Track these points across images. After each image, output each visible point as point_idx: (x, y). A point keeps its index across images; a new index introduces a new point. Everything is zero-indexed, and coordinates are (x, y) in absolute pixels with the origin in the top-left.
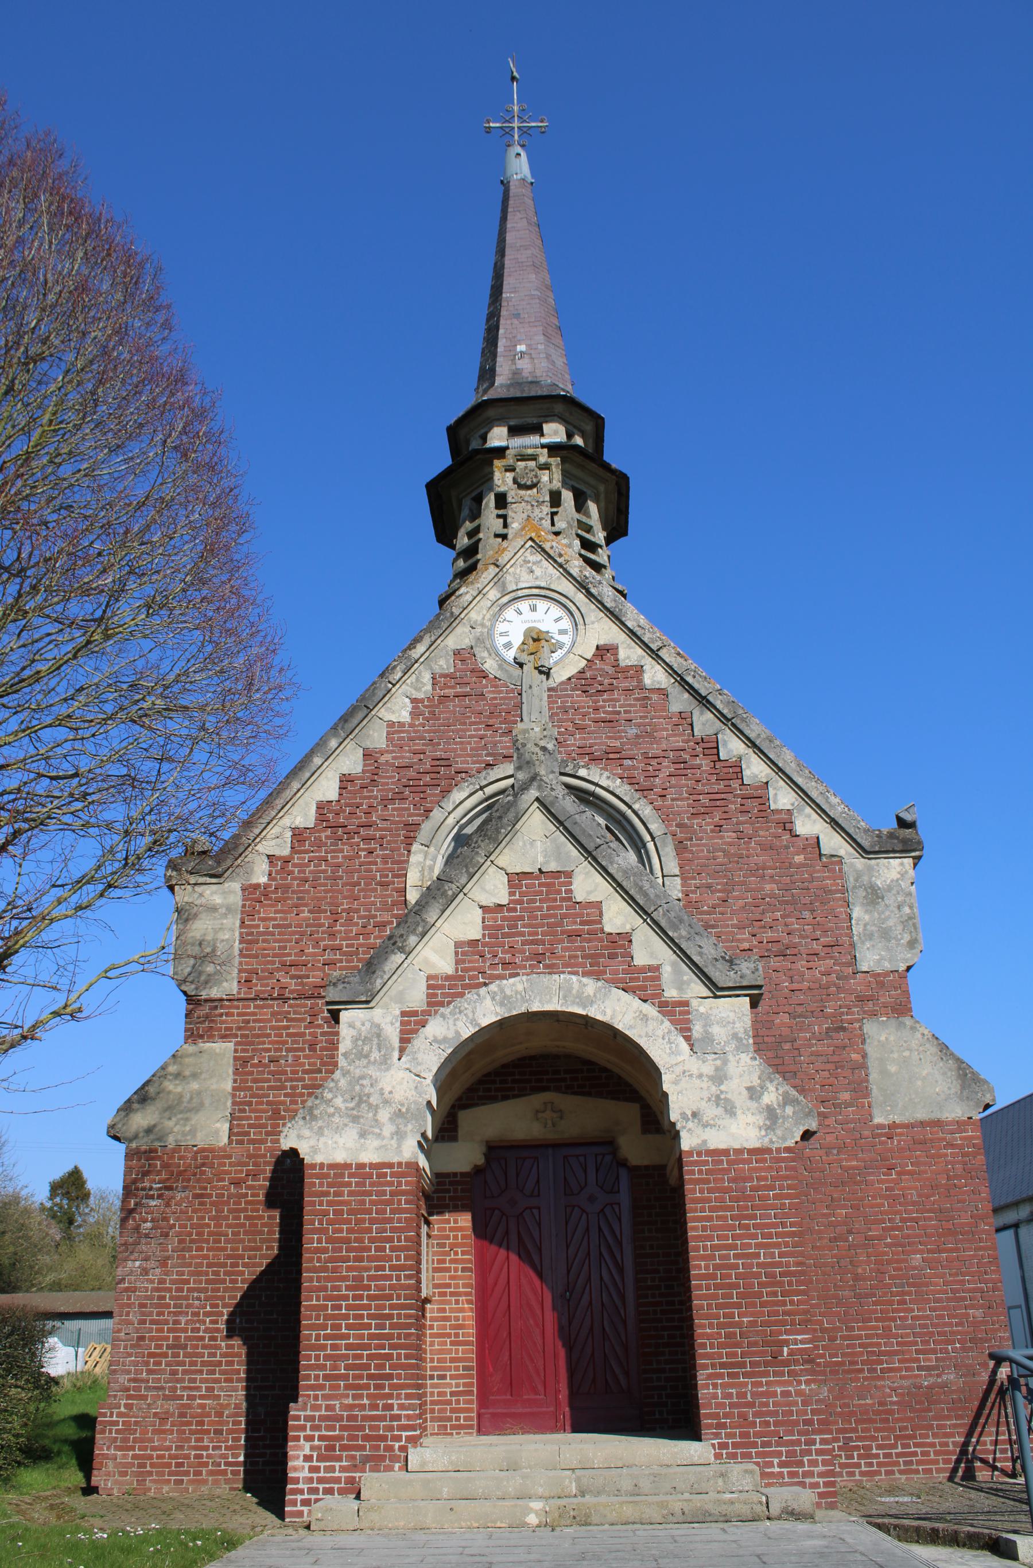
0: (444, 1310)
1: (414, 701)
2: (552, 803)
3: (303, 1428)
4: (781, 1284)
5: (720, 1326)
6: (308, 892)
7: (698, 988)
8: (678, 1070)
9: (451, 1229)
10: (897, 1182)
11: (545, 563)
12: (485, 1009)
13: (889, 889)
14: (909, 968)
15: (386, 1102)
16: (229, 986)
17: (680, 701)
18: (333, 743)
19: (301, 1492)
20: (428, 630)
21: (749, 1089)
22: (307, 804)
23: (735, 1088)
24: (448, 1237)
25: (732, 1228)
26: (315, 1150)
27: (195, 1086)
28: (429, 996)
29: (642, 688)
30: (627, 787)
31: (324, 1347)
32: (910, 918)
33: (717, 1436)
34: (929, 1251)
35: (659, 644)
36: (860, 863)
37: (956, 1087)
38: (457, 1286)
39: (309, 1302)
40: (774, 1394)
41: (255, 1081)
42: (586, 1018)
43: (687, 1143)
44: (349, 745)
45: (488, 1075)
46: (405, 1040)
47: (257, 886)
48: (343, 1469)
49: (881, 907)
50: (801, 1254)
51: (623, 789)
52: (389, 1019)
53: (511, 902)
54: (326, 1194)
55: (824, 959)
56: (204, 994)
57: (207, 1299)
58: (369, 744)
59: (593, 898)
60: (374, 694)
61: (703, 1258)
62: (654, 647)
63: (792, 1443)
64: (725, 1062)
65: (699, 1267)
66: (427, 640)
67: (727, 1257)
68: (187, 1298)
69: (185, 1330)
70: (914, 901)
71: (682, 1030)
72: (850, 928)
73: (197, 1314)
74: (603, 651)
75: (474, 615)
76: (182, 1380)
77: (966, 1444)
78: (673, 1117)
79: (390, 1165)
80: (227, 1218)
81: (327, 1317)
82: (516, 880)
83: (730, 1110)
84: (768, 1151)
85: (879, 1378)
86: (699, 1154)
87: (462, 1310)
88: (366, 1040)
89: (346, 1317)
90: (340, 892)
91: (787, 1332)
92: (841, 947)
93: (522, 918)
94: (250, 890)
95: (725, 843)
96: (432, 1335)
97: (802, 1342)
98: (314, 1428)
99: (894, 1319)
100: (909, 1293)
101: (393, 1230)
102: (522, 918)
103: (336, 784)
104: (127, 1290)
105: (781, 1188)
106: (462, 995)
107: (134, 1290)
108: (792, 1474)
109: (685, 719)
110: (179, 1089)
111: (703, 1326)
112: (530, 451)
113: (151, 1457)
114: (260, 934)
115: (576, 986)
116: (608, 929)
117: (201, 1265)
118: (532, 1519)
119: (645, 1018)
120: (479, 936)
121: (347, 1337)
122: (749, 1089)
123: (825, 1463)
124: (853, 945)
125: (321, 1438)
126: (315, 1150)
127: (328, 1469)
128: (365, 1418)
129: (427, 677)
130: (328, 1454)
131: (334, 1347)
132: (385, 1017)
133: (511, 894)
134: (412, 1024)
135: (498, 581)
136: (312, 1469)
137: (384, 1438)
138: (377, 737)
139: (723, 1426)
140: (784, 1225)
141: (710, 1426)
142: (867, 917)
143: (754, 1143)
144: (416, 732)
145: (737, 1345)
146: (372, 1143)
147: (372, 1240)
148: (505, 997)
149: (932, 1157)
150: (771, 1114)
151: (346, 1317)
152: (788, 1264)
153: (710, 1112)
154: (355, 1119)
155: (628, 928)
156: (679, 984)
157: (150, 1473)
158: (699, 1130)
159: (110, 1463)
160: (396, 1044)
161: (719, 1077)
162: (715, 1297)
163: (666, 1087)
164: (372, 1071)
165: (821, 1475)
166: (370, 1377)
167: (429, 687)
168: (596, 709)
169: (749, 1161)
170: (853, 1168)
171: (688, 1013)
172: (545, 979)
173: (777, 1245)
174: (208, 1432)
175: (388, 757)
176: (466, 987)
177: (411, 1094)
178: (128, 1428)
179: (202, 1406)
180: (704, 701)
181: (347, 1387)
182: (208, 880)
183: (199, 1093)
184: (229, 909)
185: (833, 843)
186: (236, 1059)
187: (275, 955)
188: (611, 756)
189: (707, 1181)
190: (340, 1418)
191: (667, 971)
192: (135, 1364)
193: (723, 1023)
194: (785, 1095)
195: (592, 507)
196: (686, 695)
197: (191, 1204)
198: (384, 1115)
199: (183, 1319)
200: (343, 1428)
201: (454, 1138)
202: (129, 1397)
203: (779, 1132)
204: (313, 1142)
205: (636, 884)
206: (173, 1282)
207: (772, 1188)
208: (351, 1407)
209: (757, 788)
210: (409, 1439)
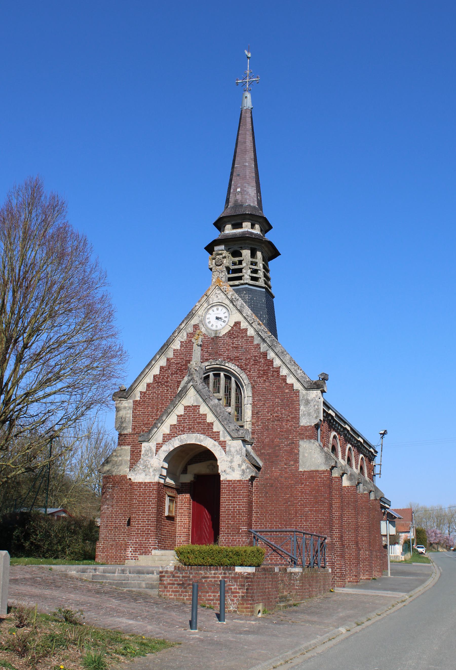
0: (181, 519)
1: (181, 342)
2: (196, 386)
3: (130, 545)
5: (226, 524)
6: (150, 402)
7: (229, 438)
8: (222, 459)
9: (184, 498)
10: (303, 487)
12: (176, 443)
13: (312, 400)
15: (152, 467)
16: (129, 430)
17: (257, 340)
18: (158, 357)
23: (235, 464)
24: (183, 500)
25: (231, 500)
26: (135, 479)
27: (120, 458)
28: (163, 439)
30: (239, 369)
31: (135, 527)
32: (317, 409)
34: (311, 507)
35: (252, 321)
36: (304, 392)
37: (324, 460)
38: (185, 513)
41: (136, 457)
42: (201, 445)
44: (163, 357)
47: (137, 401)
52: (153, 445)
53: (184, 414)
55: (290, 422)
56: (123, 433)
57: (123, 515)
60: (169, 341)
61: (223, 507)
62: (251, 322)
64: (233, 457)
68: (118, 515)
69: (118, 524)
71: (224, 449)
73: (120, 519)
74: (237, 324)
75: (200, 313)
76: (117, 536)
78: (219, 471)
79: (152, 483)
80: (128, 494)
83: (233, 470)
84: (242, 481)
86: (225, 481)
87: (186, 519)
88: (148, 451)
89: (141, 519)
90: (159, 402)
91: (242, 526)
92: (296, 418)
93: (187, 418)
94: (135, 402)
95: (266, 386)
96: (178, 526)
99: (298, 526)
100: (303, 519)
101: (152, 499)
102: (187, 418)
104: (103, 513)
105: (244, 490)
106: (171, 439)
107: (105, 513)
110: (116, 459)
112: (220, 252)
113: (109, 555)
114: (138, 415)
115: (199, 437)
116: (207, 421)
117: (121, 507)
119: (215, 445)
120: (176, 423)
121: (141, 524)
124: (299, 418)
125: (134, 547)
126: (135, 479)
127: (135, 554)
128: (143, 543)
129: (185, 334)
132: (152, 445)
133: (185, 412)
134: (159, 447)
136: (132, 554)
137: (147, 548)
138: (170, 354)
142: (304, 409)
143: (238, 479)
144: (181, 352)
145: (230, 529)
146: (148, 477)
147: (147, 501)
148: (181, 440)
149: (314, 481)
150: (243, 471)
151: (141, 519)
153: (228, 470)
154: (144, 471)
155: (212, 421)
157: (109, 559)
158: (225, 475)
159: (100, 557)
160: (155, 452)
161: (231, 462)
164: (149, 459)
166: (146, 534)
167: (186, 337)
171: (226, 444)
172: (191, 435)
174: (123, 549)
175: (173, 361)
176: (172, 437)
177: (158, 465)
178: (104, 548)
179: (121, 543)
180: (264, 340)
181: (140, 536)
182: (123, 399)
183: (121, 460)
184: (129, 408)
186: (131, 451)
187: (141, 421)
188: (236, 359)
189: (226, 488)
190: (138, 543)
191: (221, 433)
192: (106, 532)
193: (234, 447)
194: (247, 466)
195: (259, 254)
196: (259, 338)
197: (119, 491)
198: (151, 470)
199: (117, 521)
201: (186, 473)
202: (104, 540)
203: (245, 476)
204: (134, 477)
205: (215, 409)
206: (115, 511)
208: (141, 540)
209: (276, 368)
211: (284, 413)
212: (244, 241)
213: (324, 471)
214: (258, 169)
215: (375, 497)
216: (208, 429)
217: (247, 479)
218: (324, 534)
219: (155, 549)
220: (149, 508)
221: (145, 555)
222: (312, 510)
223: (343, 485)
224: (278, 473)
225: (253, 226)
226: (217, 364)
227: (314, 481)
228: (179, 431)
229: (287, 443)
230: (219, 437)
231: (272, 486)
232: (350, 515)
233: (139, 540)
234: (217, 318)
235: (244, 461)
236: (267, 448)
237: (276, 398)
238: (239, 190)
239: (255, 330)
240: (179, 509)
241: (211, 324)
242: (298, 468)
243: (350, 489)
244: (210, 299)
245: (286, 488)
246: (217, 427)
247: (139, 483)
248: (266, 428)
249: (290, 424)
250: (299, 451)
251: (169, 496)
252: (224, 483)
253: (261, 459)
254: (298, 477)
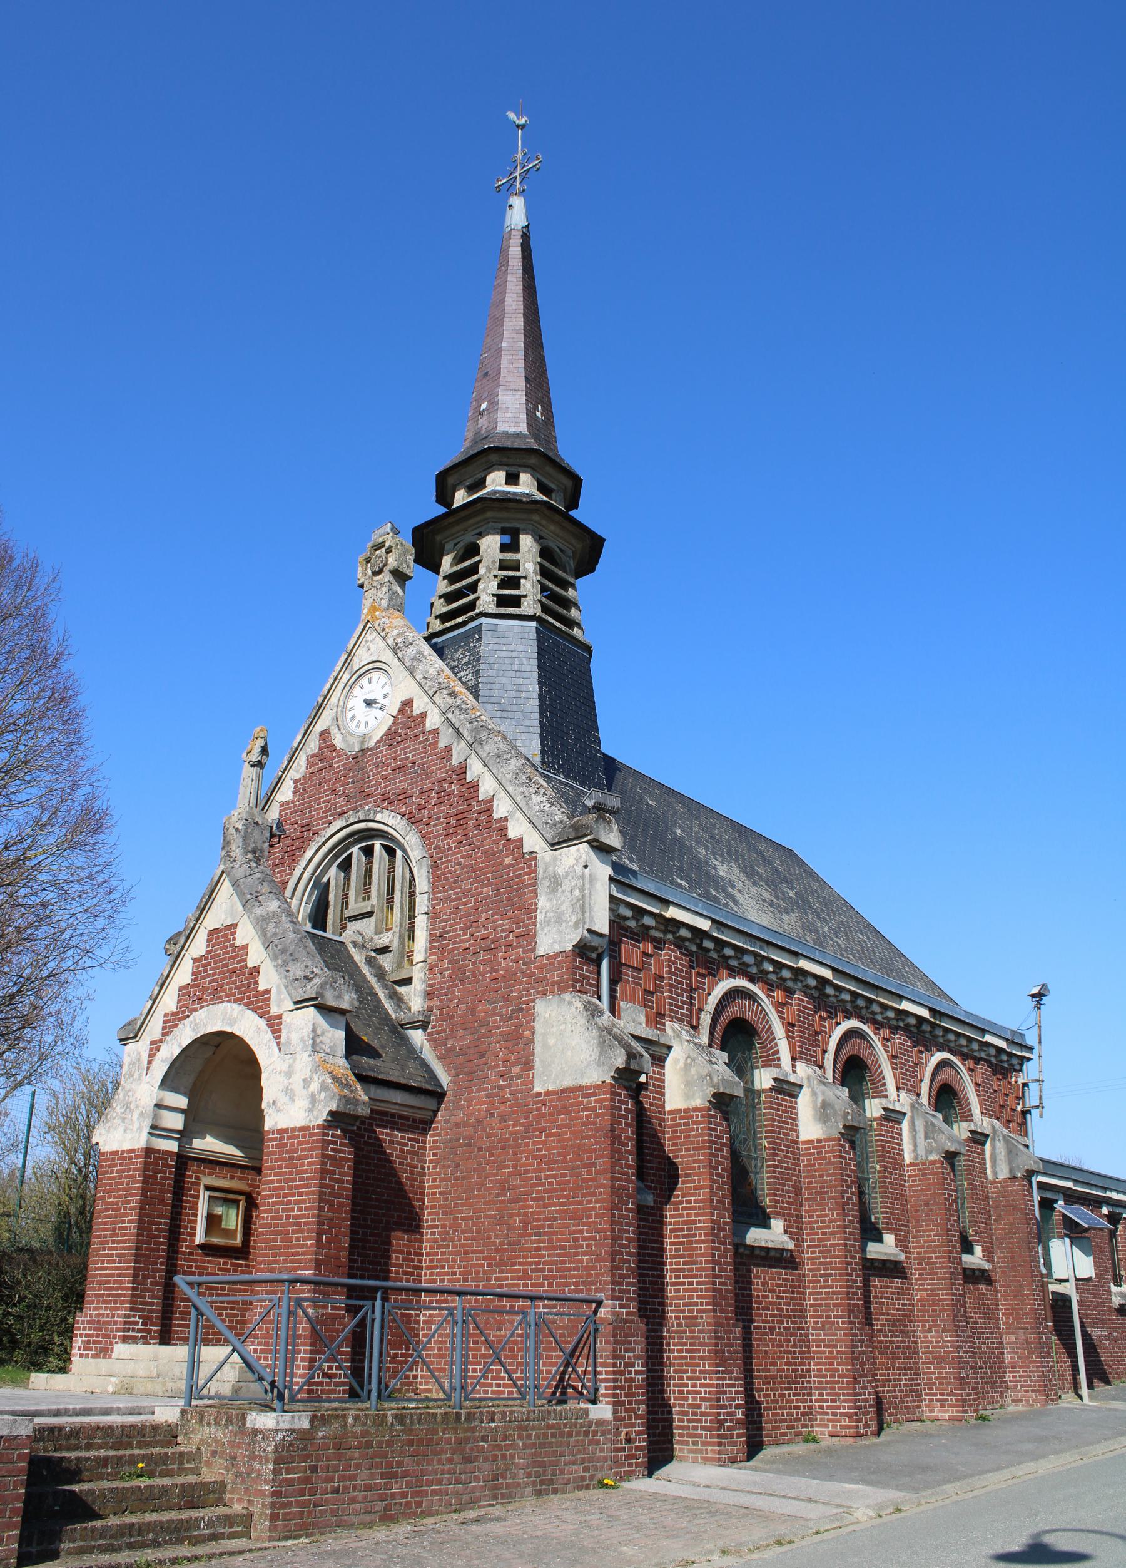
10: (544, 1143)
12: (185, 1035)
13: (567, 874)
23: (297, 1081)
26: (105, 1143)
34: (562, 1204)
35: (435, 689)
49: (559, 894)
74: (407, 704)
77: (564, 1373)
92: (528, 936)
118: (110, 1389)
122: (304, 1080)
124: (535, 936)
133: (208, 946)
134: (155, 1046)
142: (548, 905)
143: (301, 1123)
146: (129, 1136)
148: (196, 1024)
153: (283, 1099)
161: (289, 1074)
163: (263, 1084)
171: (280, 1023)
195: (526, 542)
198: (136, 1115)
203: (315, 1113)
211: (502, 925)
212: (511, 525)
213: (597, 1087)
214: (547, 354)
215: (1011, 1171)
218: (596, 1291)
219: (125, 1339)
222: (566, 1212)
223: (804, 1136)
224: (485, 1102)
225: (512, 479)
226: (359, 822)
227: (571, 1119)
229: (507, 1011)
231: (469, 1145)
232: (829, 1227)
234: (369, 703)
235: (315, 1070)
236: (460, 1033)
237: (484, 886)
238: (484, 406)
241: (355, 722)
242: (532, 1083)
243: (824, 1147)
245: (503, 1148)
246: (269, 978)
248: (459, 976)
250: (533, 1033)
251: (208, 1188)
253: (447, 1069)
254: (531, 1110)
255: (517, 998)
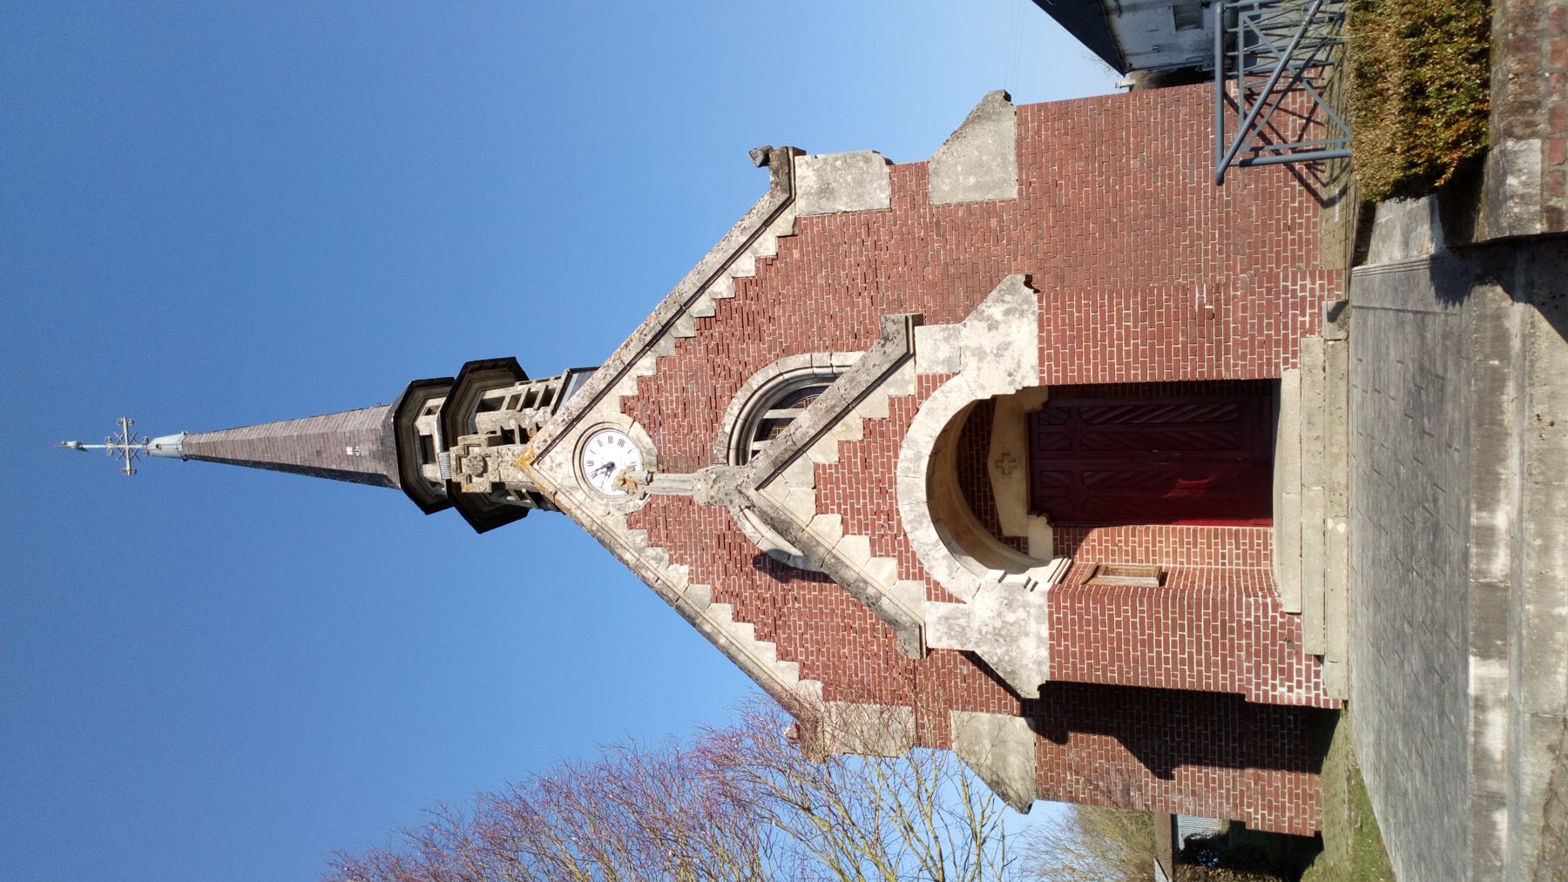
3: (1266, 692)
4: (1152, 309)
7: (907, 369)
11: (552, 453)
12: (924, 535)
13: (820, 177)
14: (889, 162)
15: (999, 615)
17: (666, 345)
19: (1317, 696)
20: (612, 552)
21: (990, 329)
22: (757, 648)
23: (988, 341)
29: (656, 378)
30: (739, 393)
31: (1199, 672)
33: (1277, 366)
39: (1162, 681)
40: (1244, 318)
43: (1033, 382)
45: (973, 510)
46: (951, 599)
47: (824, 689)
48: (1299, 662)
50: (1127, 291)
51: (741, 397)
52: (933, 610)
54: (1074, 664)
58: (707, 599)
59: (836, 448)
63: (1286, 305)
64: (967, 347)
65: (1136, 375)
66: (620, 551)
67: (1128, 352)
70: (831, 157)
72: (853, 213)
74: (626, 407)
78: (1012, 391)
79: (1051, 614)
81: (1175, 668)
82: (821, 508)
85: (1235, 200)
86: (1042, 372)
88: (950, 628)
89: (1174, 654)
92: (868, 221)
97: (1201, 293)
98: (1266, 683)
99: (1185, 185)
103: (741, 625)
105: (1071, 306)
106: (914, 554)
108: (1312, 306)
109: (682, 343)
111: (1185, 373)
115: (906, 464)
116: (860, 437)
121: (1191, 654)
122: (990, 329)
123: (1303, 279)
124: (869, 212)
125: (1274, 678)
128: (1257, 643)
129: (651, 552)
130: (1287, 674)
131: (1199, 664)
132: (932, 615)
134: (937, 593)
135: (569, 491)
137: (1274, 629)
138: (703, 591)
139: (1269, 360)
140: (1102, 306)
141: (1269, 371)
143: (1034, 327)
147: (1111, 631)
149: (1047, 147)
151: (1174, 654)
152: (1136, 303)
153: (1007, 363)
156: (904, 382)
158: (1022, 372)
160: (954, 605)
161: (980, 354)
162: (1160, 363)
163: (987, 396)
164: (975, 624)
165: (1313, 282)
166: (1223, 637)
168: (675, 416)
169: (1049, 332)
170: (1054, 217)
172: (900, 487)
173: (1119, 311)
175: (718, 584)
181: (1232, 655)
185: (783, 224)
189: (1065, 366)
190: (1258, 664)
191: (893, 392)
193: (936, 348)
200: (1266, 661)
201: (1026, 540)
207: (1071, 314)
208: (1249, 654)
210: (1274, 610)
216: (882, 434)
217: (1035, 297)
220: (1134, 624)
221: (1299, 638)
228: (890, 527)
230: (906, 398)
233: (1249, 659)
237: (815, 285)
239: (641, 353)
240: (1134, 560)
244: (566, 483)
247: (1052, 659)
249: (884, 237)
250: (961, 205)
252: (1050, 375)
255: (926, 229)
